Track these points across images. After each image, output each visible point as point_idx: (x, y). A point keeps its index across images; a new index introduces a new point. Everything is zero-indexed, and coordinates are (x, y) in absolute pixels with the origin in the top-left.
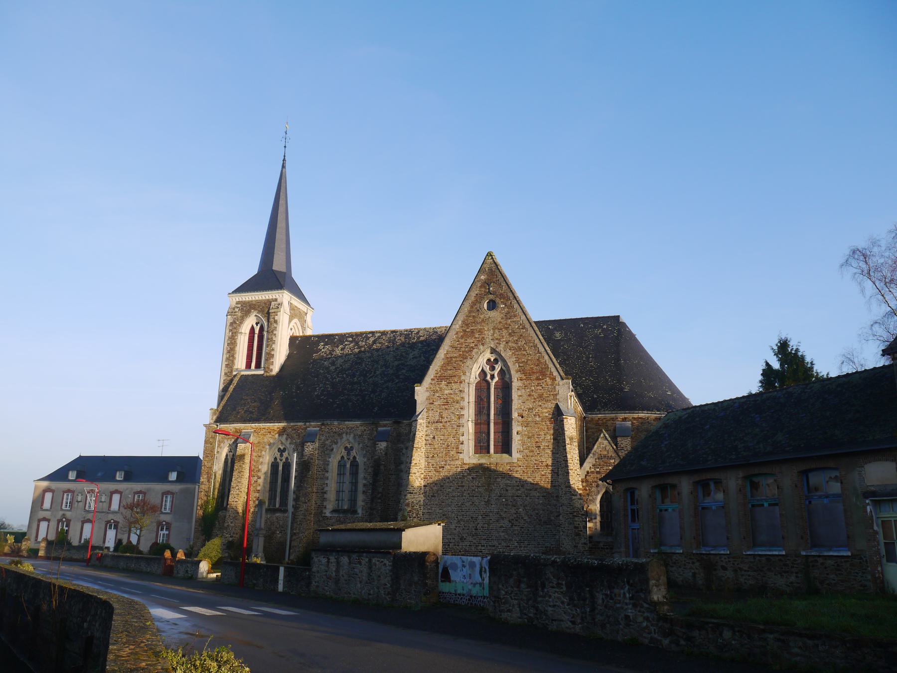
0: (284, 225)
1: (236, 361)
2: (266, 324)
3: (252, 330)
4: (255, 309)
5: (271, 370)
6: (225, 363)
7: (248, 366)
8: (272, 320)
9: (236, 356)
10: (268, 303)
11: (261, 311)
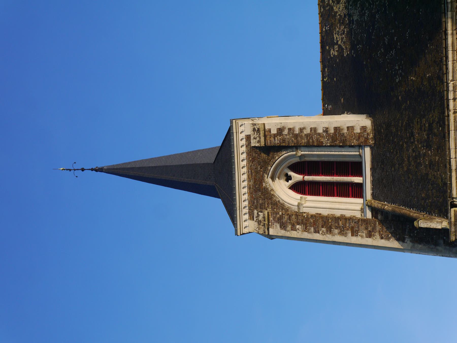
0: (350, 151)
1: (348, 214)
2: (285, 154)
3: (298, 188)
4: (262, 180)
5: (364, 128)
6: (281, 201)
7: (356, 191)
8: (277, 141)
9: (338, 213)
10: (253, 151)
11: (265, 165)
